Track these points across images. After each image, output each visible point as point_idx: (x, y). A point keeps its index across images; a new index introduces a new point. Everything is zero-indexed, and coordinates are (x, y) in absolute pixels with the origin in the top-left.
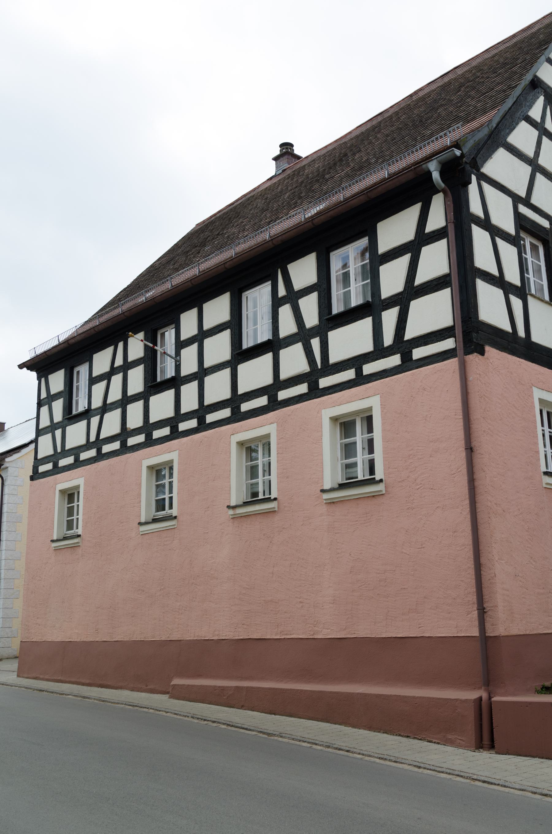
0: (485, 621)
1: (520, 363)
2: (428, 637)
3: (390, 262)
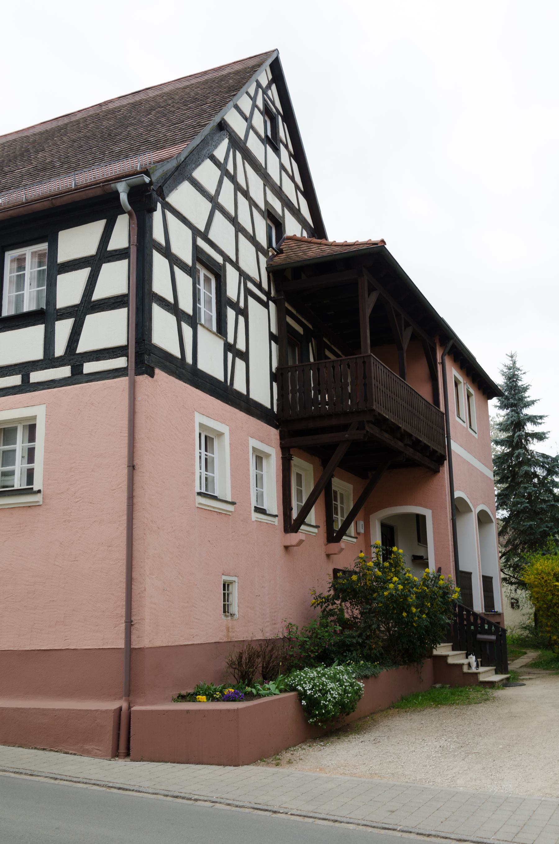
0: (132, 634)
1: (186, 388)
2: (74, 649)
3: (68, 273)
